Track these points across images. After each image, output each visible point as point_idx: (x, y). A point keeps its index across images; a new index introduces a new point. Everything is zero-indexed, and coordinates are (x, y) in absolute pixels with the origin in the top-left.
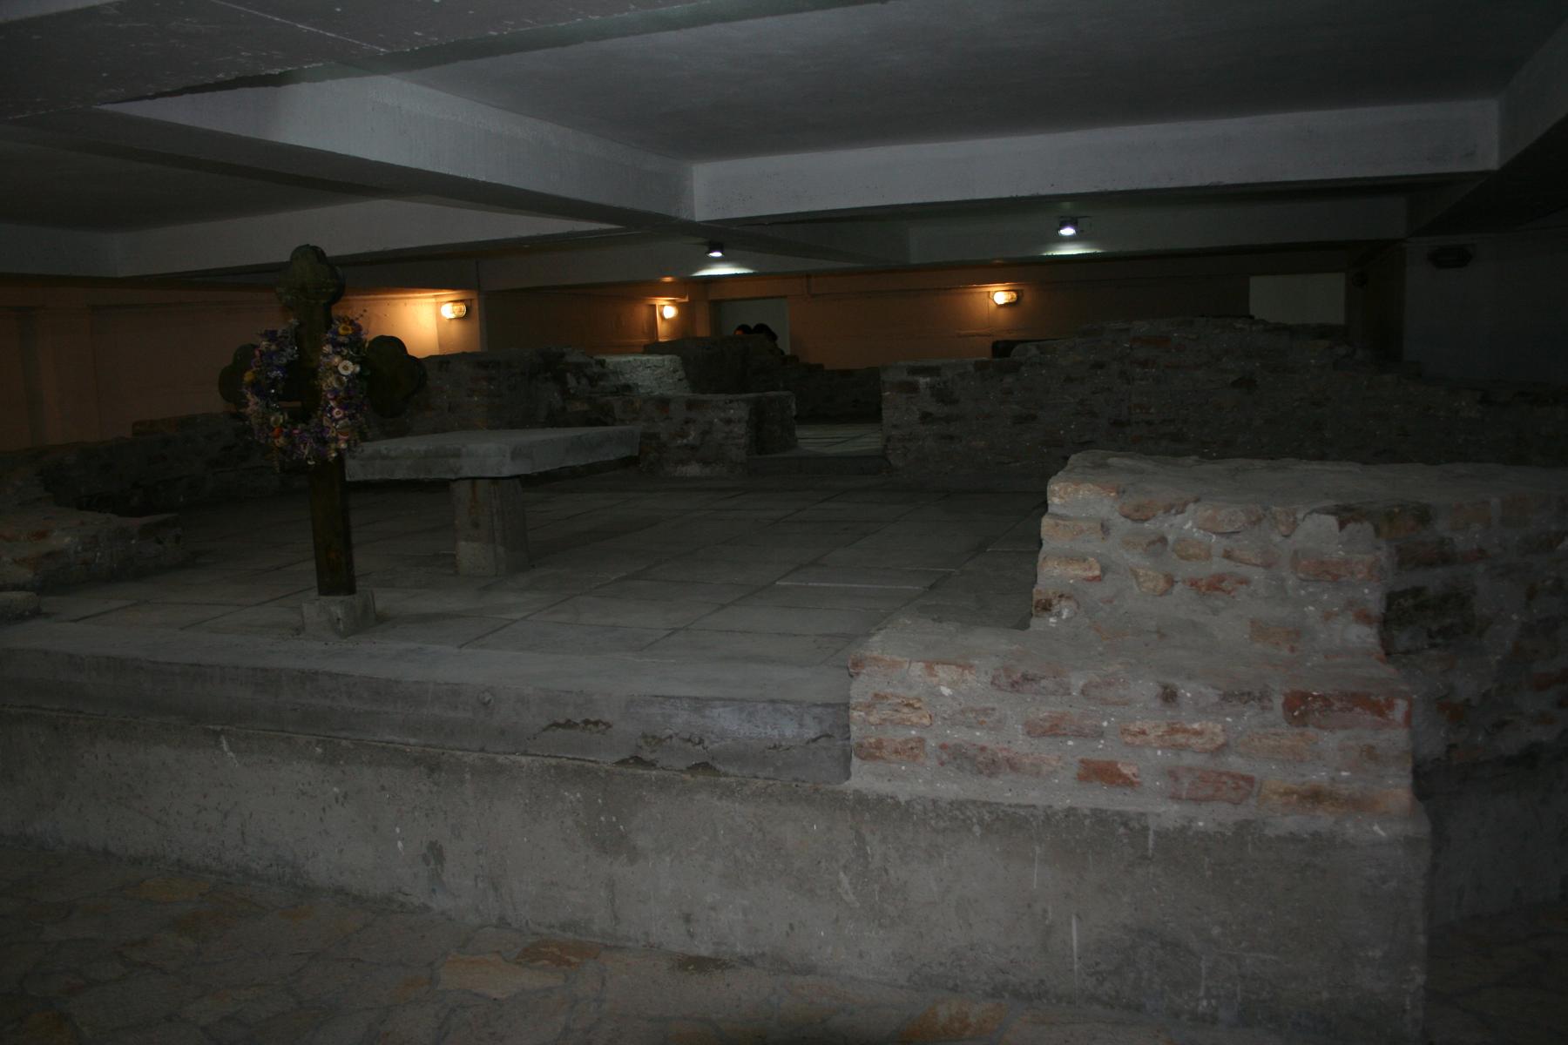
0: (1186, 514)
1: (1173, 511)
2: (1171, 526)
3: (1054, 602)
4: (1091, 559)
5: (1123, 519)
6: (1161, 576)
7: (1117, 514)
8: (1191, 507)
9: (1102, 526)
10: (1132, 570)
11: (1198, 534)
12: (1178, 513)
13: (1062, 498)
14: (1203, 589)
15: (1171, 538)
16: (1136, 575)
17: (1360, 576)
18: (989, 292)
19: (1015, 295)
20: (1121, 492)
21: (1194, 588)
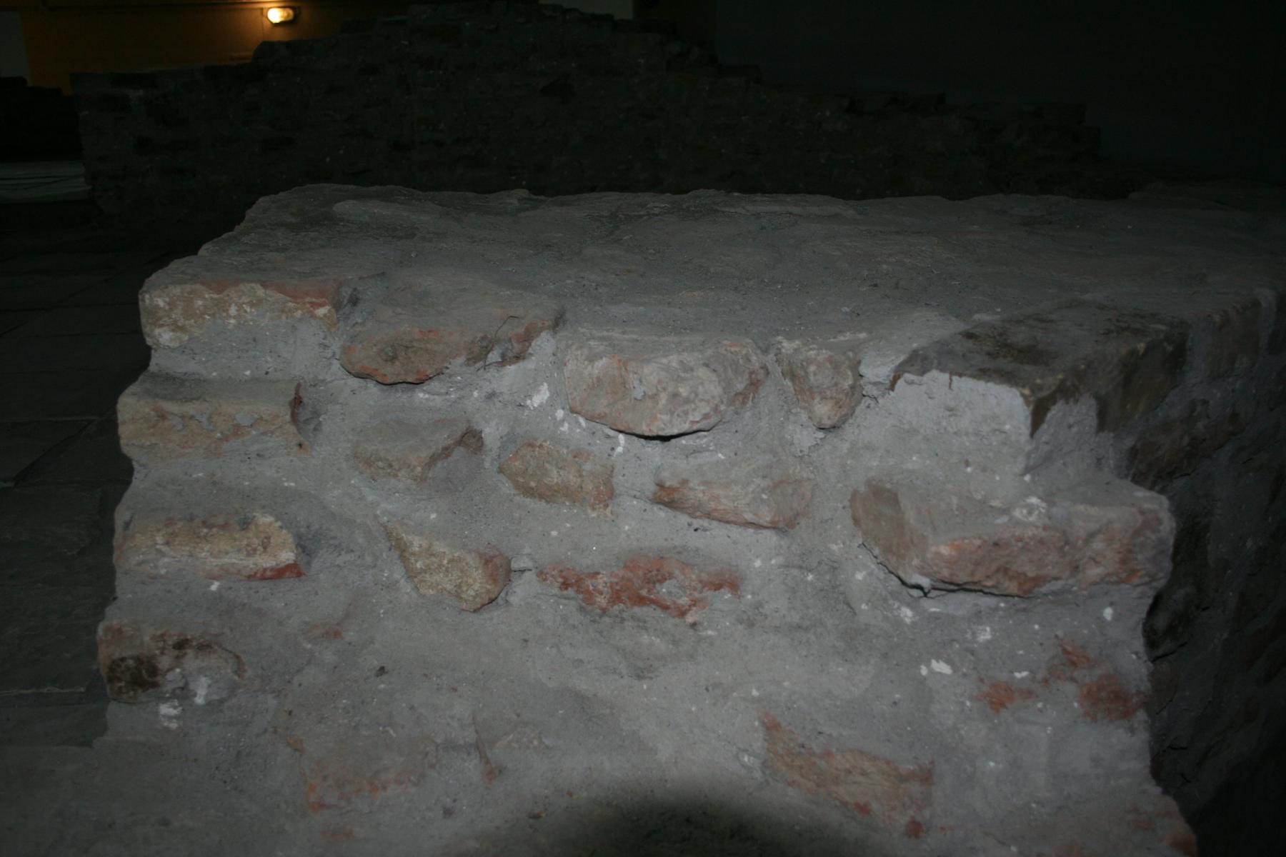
0: (530, 364)
1: (494, 356)
2: (491, 396)
3: (164, 662)
4: (265, 520)
5: (355, 382)
6: (472, 560)
7: (336, 365)
8: (544, 344)
9: (297, 402)
10: (389, 535)
11: (571, 429)
12: (504, 361)
13: (182, 329)
14: (602, 601)
15: (491, 432)
16: (401, 549)
17: (1095, 572)
18: (262, 9)
19: (291, 12)
20: (346, 303)
21: (571, 592)
